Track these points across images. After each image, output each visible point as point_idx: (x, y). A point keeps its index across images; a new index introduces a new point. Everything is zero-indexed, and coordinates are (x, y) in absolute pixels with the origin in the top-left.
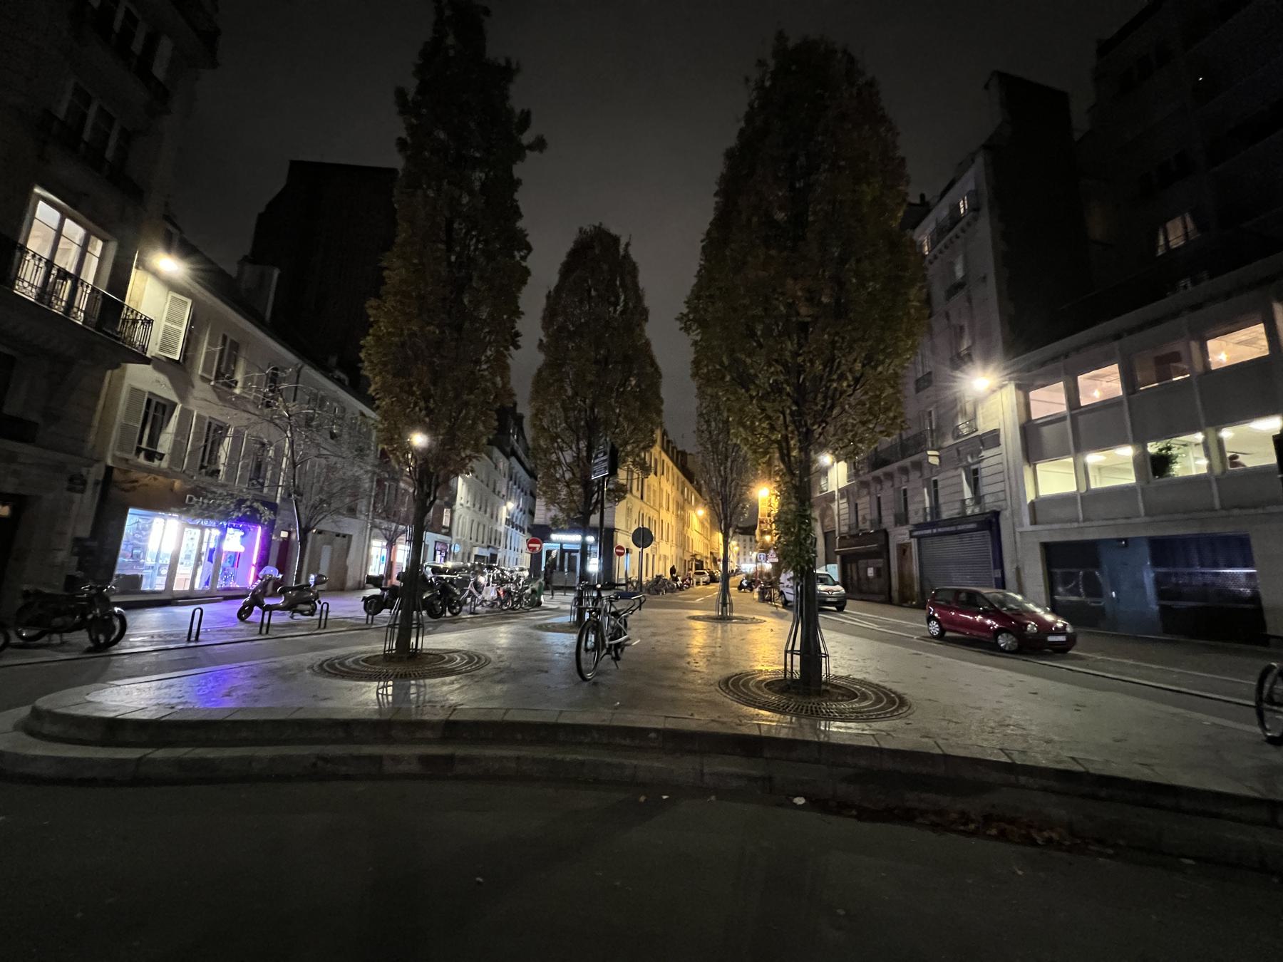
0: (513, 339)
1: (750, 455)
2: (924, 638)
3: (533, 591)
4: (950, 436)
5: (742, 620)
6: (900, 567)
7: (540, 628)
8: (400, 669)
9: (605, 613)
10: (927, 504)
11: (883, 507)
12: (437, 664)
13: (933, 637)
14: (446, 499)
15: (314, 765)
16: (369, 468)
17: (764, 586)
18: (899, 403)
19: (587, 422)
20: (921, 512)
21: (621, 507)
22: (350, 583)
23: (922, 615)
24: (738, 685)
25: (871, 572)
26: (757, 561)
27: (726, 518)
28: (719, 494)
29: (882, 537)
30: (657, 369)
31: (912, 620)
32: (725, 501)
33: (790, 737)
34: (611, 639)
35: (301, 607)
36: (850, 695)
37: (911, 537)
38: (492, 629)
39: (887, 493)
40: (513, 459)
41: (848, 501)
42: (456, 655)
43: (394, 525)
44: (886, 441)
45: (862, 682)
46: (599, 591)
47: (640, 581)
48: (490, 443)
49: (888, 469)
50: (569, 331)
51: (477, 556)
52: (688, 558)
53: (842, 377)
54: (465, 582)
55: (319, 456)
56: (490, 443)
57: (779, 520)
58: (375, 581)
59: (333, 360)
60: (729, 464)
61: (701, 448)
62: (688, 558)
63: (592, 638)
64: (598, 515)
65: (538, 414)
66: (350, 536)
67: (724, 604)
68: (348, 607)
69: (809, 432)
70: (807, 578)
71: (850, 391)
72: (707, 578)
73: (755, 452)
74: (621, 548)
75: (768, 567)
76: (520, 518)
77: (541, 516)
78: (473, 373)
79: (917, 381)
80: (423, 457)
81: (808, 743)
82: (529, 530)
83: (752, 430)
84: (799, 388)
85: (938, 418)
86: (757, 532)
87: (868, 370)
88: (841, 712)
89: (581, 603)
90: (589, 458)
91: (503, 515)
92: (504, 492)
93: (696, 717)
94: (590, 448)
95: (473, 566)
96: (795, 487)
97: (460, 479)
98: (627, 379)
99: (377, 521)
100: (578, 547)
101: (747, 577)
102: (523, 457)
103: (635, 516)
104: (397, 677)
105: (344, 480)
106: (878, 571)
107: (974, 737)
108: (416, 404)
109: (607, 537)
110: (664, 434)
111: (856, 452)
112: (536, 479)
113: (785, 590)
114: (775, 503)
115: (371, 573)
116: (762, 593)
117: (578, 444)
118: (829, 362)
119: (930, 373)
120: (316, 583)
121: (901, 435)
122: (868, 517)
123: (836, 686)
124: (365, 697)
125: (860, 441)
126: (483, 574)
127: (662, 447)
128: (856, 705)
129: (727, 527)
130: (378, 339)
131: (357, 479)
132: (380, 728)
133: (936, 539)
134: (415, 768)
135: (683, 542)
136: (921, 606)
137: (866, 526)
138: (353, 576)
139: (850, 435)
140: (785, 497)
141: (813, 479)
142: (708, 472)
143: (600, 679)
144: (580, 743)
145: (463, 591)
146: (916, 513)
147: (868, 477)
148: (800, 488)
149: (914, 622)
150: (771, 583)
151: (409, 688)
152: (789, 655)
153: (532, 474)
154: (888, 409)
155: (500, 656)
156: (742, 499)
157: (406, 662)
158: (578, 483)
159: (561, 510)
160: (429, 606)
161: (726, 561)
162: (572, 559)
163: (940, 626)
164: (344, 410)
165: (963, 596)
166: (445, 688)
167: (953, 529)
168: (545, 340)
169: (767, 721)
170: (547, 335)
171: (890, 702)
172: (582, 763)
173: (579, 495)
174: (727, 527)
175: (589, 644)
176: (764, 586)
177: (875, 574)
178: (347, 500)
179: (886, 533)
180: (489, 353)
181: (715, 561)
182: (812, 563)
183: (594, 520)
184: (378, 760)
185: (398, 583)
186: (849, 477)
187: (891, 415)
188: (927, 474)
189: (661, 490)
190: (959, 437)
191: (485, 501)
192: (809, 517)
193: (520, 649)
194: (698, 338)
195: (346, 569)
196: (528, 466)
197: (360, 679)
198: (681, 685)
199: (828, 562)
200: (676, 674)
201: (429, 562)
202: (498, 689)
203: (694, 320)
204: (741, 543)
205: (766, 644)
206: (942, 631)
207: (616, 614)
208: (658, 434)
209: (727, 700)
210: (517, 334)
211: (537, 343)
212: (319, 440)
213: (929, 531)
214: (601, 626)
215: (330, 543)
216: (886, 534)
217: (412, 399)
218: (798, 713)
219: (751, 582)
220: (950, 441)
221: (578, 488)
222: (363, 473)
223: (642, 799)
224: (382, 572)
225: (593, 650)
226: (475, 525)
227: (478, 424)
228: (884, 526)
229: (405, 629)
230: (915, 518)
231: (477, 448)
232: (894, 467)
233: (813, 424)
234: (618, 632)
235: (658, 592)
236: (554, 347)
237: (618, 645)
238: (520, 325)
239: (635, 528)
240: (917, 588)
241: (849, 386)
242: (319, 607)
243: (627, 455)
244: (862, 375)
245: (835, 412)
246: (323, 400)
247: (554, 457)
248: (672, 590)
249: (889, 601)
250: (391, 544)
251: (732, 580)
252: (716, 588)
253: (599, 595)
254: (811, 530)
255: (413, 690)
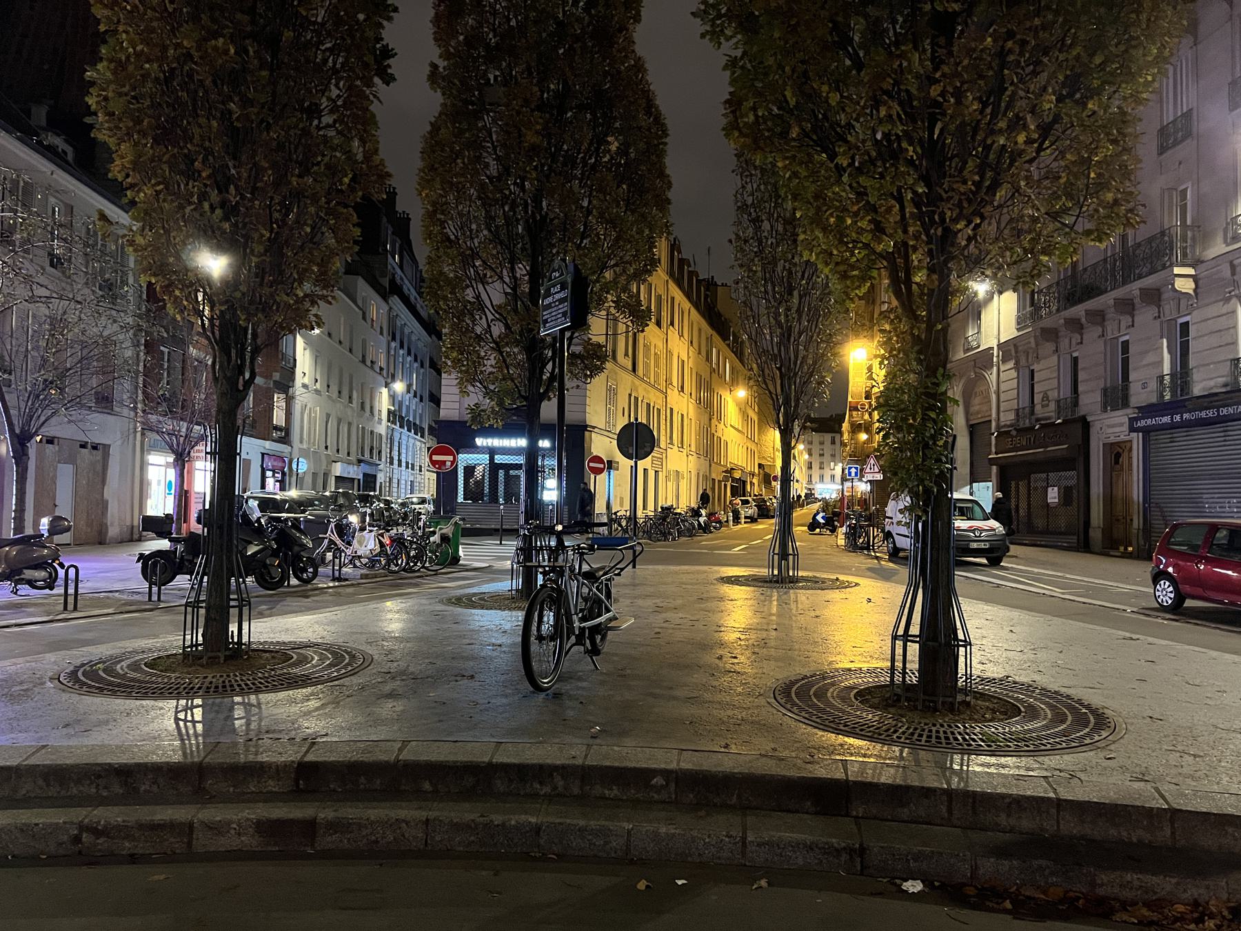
0: (379, 62)
1: (835, 285)
2: (1146, 611)
3: (444, 538)
4: (1219, 239)
5: (817, 584)
6: (1109, 485)
7: (458, 601)
8: (213, 676)
9: (572, 572)
10: (1167, 369)
11: (1082, 376)
12: (280, 668)
13: (1163, 609)
14: (276, 376)
15: (77, 839)
16: (130, 320)
17: (855, 522)
18: (1126, 174)
19: (527, 228)
20: (1153, 385)
21: (597, 387)
22: (113, 531)
23: (1144, 570)
24: (809, 695)
25: (1053, 495)
26: (844, 480)
27: (787, 402)
28: (775, 358)
29: (1078, 427)
30: (658, 121)
31: (1126, 580)
32: (787, 375)
33: (899, 781)
34: (583, 620)
35: (28, 574)
36: (1008, 709)
37: (1132, 429)
38: (372, 605)
39: (1092, 350)
40: (395, 300)
41: (1017, 367)
42: (309, 652)
43: (184, 425)
44: (1094, 251)
45: (1029, 688)
46: (559, 536)
47: (633, 518)
48: (350, 270)
49: (1092, 304)
50: (487, 46)
51: (339, 479)
52: (717, 475)
53: (1017, 124)
54: (320, 525)
55: (32, 299)
56: (350, 270)
57: (886, 402)
58: (158, 526)
59: (40, 114)
60: (796, 301)
61: (740, 273)
62: (717, 475)
63: (549, 617)
64: (555, 401)
65: (436, 213)
66: (106, 447)
67: (784, 555)
68: (113, 572)
69: (948, 235)
70: (935, 507)
71: (1031, 151)
72: (752, 511)
73: (844, 276)
74: (598, 459)
75: (863, 487)
76: (415, 410)
77: (453, 404)
78: (306, 132)
79: (1163, 132)
80: (227, 297)
81: (928, 792)
82: (432, 431)
83: (840, 234)
84: (933, 150)
85: (1199, 199)
86: (845, 426)
87: (1069, 109)
88: (989, 740)
89: (528, 558)
90: (534, 295)
91: (384, 403)
92: (382, 362)
93: (733, 749)
94: (536, 277)
95: (335, 497)
96: (916, 340)
97: (300, 342)
98: (601, 141)
99: (153, 418)
100: (521, 460)
101: (826, 505)
102: (413, 294)
103: (623, 402)
104: (208, 691)
105: (84, 345)
106: (1066, 495)
107: (1226, 779)
108: (203, 196)
109: (572, 438)
110: (674, 247)
111: (1035, 274)
112: (439, 336)
113: (895, 530)
114: (880, 374)
115: (151, 512)
116: (852, 535)
117: (513, 270)
118: (993, 95)
119: (1188, 115)
120: (53, 531)
121: (1124, 238)
122: (1053, 395)
123: (982, 696)
124: (155, 726)
125: (1044, 252)
126: (353, 510)
127: (671, 274)
128: (1017, 726)
129: (789, 420)
130: (120, 66)
131: (108, 342)
132: (186, 778)
133: (1179, 434)
134: (249, 841)
135: (709, 447)
136: (1144, 555)
137: (1046, 411)
138: (117, 519)
139: (1026, 240)
140: (896, 359)
141: (954, 325)
142: (756, 318)
143: (565, 687)
144: (535, 796)
145: (318, 542)
146: (1144, 386)
147: (1057, 321)
148: (928, 344)
149: (1130, 583)
150: (869, 518)
151: (231, 709)
152: (899, 643)
153: (431, 328)
154: (1102, 185)
155: (390, 652)
156: (820, 363)
157: (221, 665)
158: (517, 343)
159: (488, 393)
160: (255, 566)
161: (787, 478)
162: (511, 481)
163: (1177, 590)
164: (70, 209)
165: (1222, 534)
166: (295, 709)
167: (1211, 413)
168: (442, 64)
169: (860, 756)
170: (446, 55)
171: (1081, 721)
172: (537, 830)
173: (518, 365)
174: (789, 420)
175: (545, 628)
176: (855, 522)
177: (1063, 493)
178: (94, 382)
179: (1085, 425)
180: (335, 92)
181: (767, 479)
182: (945, 481)
183: (548, 410)
184: (188, 829)
185: (197, 528)
186: (1021, 322)
187: (1110, 196)
188: (1168, 309)
189: (669, 353)
190: (968, 350)
191: (348, 380)
192: (943, 397)
193: (422, 639)
194: (739, 53)
195: (104, 505)
196: (423, 314)
197: (145, 696)
198: (708, 696)
199: (974, 478)
200: (698, 677)
201: (254, 489)
202: (388, 709)
203: (730, 16)
204: (816, 449)
205: (859, 622)
206: (1180, 598)
207: (591, 576)
208: (661, 249)
209: (788, 719)
210: (387, 53)
211: (427, 70)
212: (28, 268)
213: (1166, 419)
214: (562, 607)
215: (71, 460)
216: (1085, 425)
217: (195, 187)
218: (912, 741)
219: (833, 516)
220: (1218, 248)
221: (517, 353)
222: (119, 329)
223: (642, 885)
224: (170, 509)
225: (552, 638)
226: (332, 424)
227: (327, 234)
228: (1082, 411)
229: (217, 611)
230: (1141, 395)
231: (324, 280)
232: (1105, 301)
233: (955, 221)
234: (595, 606)
235: (665, 535)
236: (460, 80)
237: (596, 630)
238: (391, 34)
239: (621, 423)
240: (1137, 523)
241: (1029, 142)
242: (61, 572)
243: (606, 288)
244: (1057, 118)
245: (1000, 195)
246: (28, 190)
247: (470, 294)
248: (691, 532)
249: (1084, 546)
250: (182, 460)
251: (797, 513)
252: (768, 527)
253: (560, 543)
254: (945, 422)
255: (239, 712)
